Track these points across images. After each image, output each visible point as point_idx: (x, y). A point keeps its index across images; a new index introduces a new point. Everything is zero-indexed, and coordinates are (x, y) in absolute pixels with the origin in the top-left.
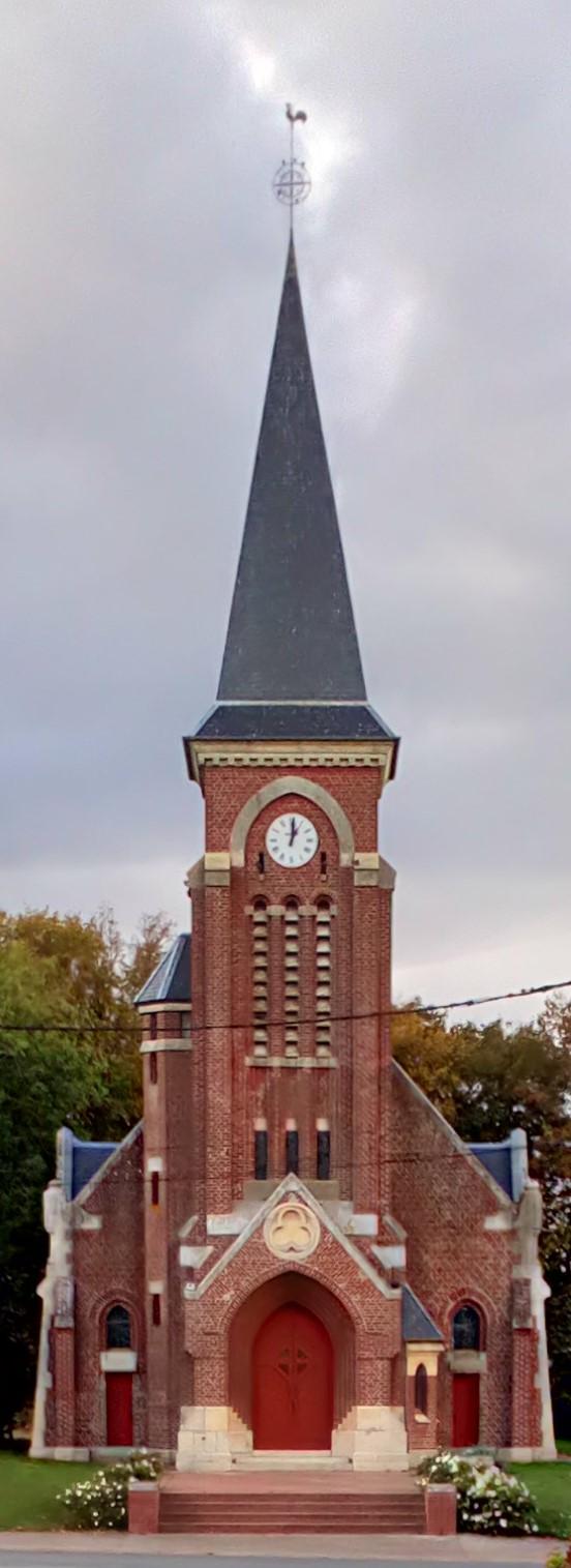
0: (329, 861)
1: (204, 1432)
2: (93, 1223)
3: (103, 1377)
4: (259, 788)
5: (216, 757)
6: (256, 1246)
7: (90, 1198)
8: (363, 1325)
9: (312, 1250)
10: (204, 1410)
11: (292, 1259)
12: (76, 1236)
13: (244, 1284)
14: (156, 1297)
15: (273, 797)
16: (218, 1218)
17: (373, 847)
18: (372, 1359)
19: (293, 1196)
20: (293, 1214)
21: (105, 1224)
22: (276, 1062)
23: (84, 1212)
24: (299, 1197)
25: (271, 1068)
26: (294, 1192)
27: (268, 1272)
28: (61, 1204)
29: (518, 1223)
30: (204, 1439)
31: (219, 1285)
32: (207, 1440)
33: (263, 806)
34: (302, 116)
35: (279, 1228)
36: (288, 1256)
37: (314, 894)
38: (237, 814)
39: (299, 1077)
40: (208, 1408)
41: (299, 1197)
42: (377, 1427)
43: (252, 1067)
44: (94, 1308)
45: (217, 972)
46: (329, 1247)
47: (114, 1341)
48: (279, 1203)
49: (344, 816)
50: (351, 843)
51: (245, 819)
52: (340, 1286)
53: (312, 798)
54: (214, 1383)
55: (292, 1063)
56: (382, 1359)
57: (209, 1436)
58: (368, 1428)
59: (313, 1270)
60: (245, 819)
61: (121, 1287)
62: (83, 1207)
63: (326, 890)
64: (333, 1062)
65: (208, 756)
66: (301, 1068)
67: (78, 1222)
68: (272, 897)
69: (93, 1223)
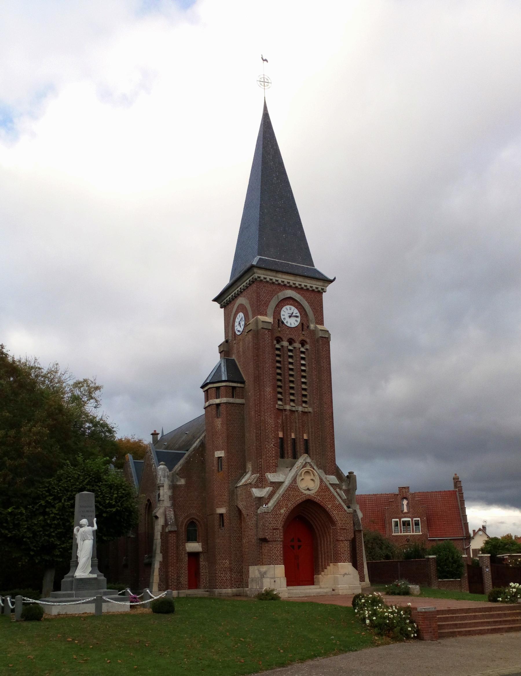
0: (305, 327)
1: (274, 578)
2: (182, 482)
3: (186, 555)
4: (278, 293)
5: (262, 277)
6: (293, 487)
7: (180, 469)
8: (339, 524)
9: (316, 490)
10: (274, 567)
11: (309, 494)
12: (174, 487)
13: (290, 505)
14: (221, 515)
15: (284, 297)
16: (272, 474)
17: (322, 323)
18: (343, 540)
19: (308, 465)
20: (307, 473)
21: (187, 482)
22: (288, 407)
23: (178, 477)
24: (311, 465)
25: (285, 410)
26: (308, 463)
27: (299, 500)
28: (167, 472)
29: (351, 487)
30: (275, 581)
31: (278, 505)
32: (276, 582)
33: (279, 301)
34: (266, 60)
35: (303, 479)
36: (307, 492)
37: (300, 339)
38: (270, 302)
39: (296, 414)
40: (276, 566)
41: (311, 465)
42: (348, 573)
43: (277, 409)
44: (182, 522)
45: (267, 365)
46: (323, 488)
47: (191, 538)
48: (303, 468)
49: (311, 310)
50: (314, 320)
51: (273, 304)
52: (329, 506)
53: (298, 300)
54: (278, 553)
55: (294, 409)
56: (347, 541)
57: (277, 580)
58: (343, 573)
59: (318, 499)
60: (273, 304)
61: (194, 512)
62: (177, 474)
63: (305, 338)
64: (310, 410)
65: (259, 275)
66: (297, 411)
67: (175, 481)
68: (284, 339)
69: (182, 482)
